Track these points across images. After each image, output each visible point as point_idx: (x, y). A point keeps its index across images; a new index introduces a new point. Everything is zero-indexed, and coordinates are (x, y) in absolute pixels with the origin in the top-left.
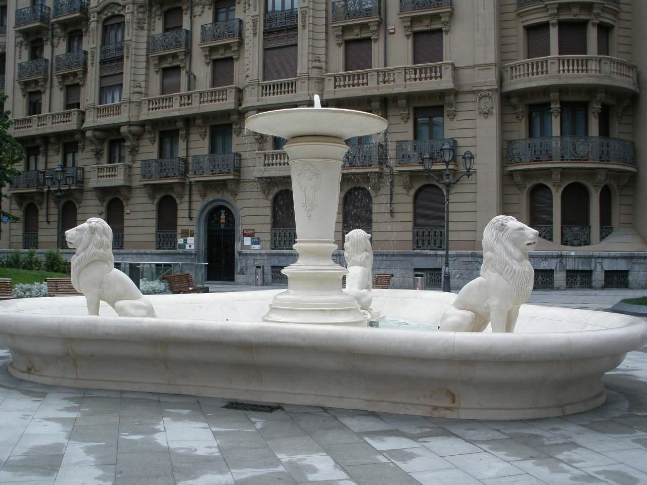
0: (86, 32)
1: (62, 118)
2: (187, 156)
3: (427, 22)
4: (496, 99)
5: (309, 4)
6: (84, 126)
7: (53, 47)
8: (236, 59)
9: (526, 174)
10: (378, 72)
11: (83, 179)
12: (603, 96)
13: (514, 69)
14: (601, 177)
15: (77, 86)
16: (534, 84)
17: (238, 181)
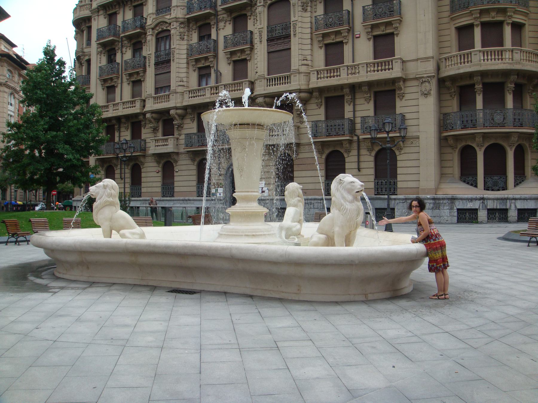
0: (250, 16)
1: (130, 105)
2: (354, 117)
3: (383, 28)
4: (434, 82)
6: (145, 110)
7: (122, 54)
8: (249, 60)
9: (457, 138)
10: (347, 66)
11: (145, 148)
12: (515, 78)
13: (447, 60)
14: (514, 139)
15: (245, 61)
16: (461, 71)
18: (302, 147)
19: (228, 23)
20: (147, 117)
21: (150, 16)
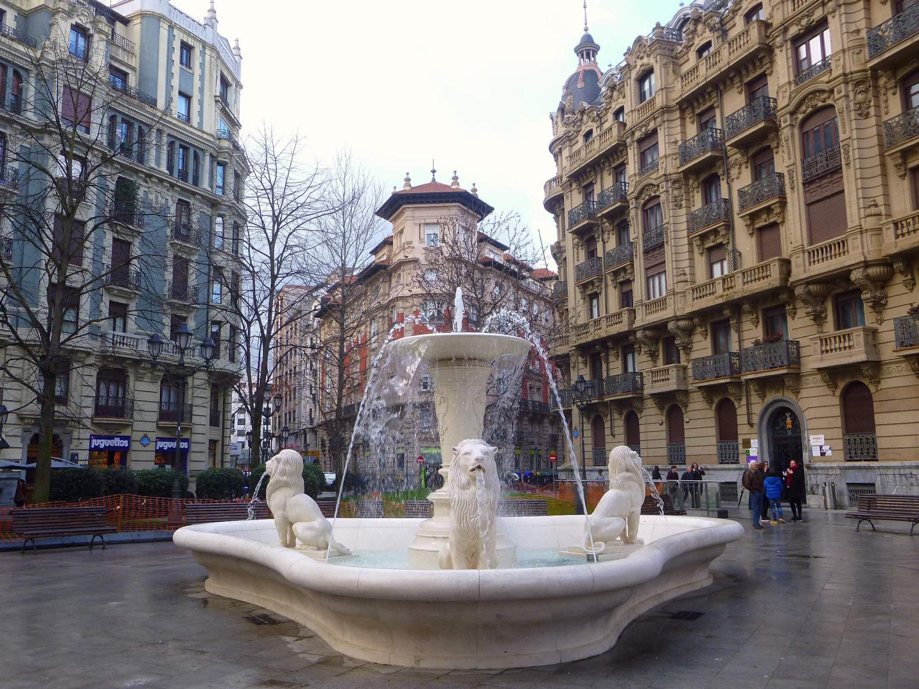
0: (777, 147)
5: (851, 133)
6: (634, 326)
7: (604, 243)
17: (797, 377)
18: (885, 367)
19: (744, 166)
20: (797, 294)
21: (784, 89)
